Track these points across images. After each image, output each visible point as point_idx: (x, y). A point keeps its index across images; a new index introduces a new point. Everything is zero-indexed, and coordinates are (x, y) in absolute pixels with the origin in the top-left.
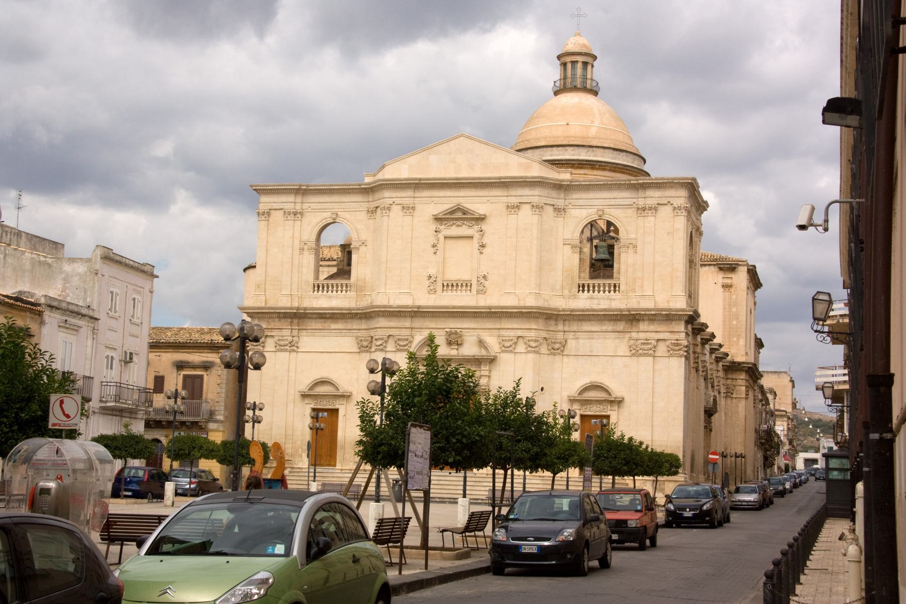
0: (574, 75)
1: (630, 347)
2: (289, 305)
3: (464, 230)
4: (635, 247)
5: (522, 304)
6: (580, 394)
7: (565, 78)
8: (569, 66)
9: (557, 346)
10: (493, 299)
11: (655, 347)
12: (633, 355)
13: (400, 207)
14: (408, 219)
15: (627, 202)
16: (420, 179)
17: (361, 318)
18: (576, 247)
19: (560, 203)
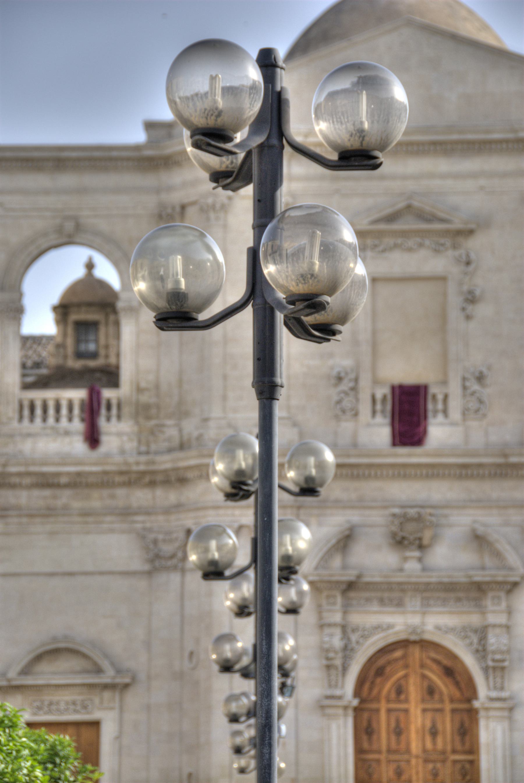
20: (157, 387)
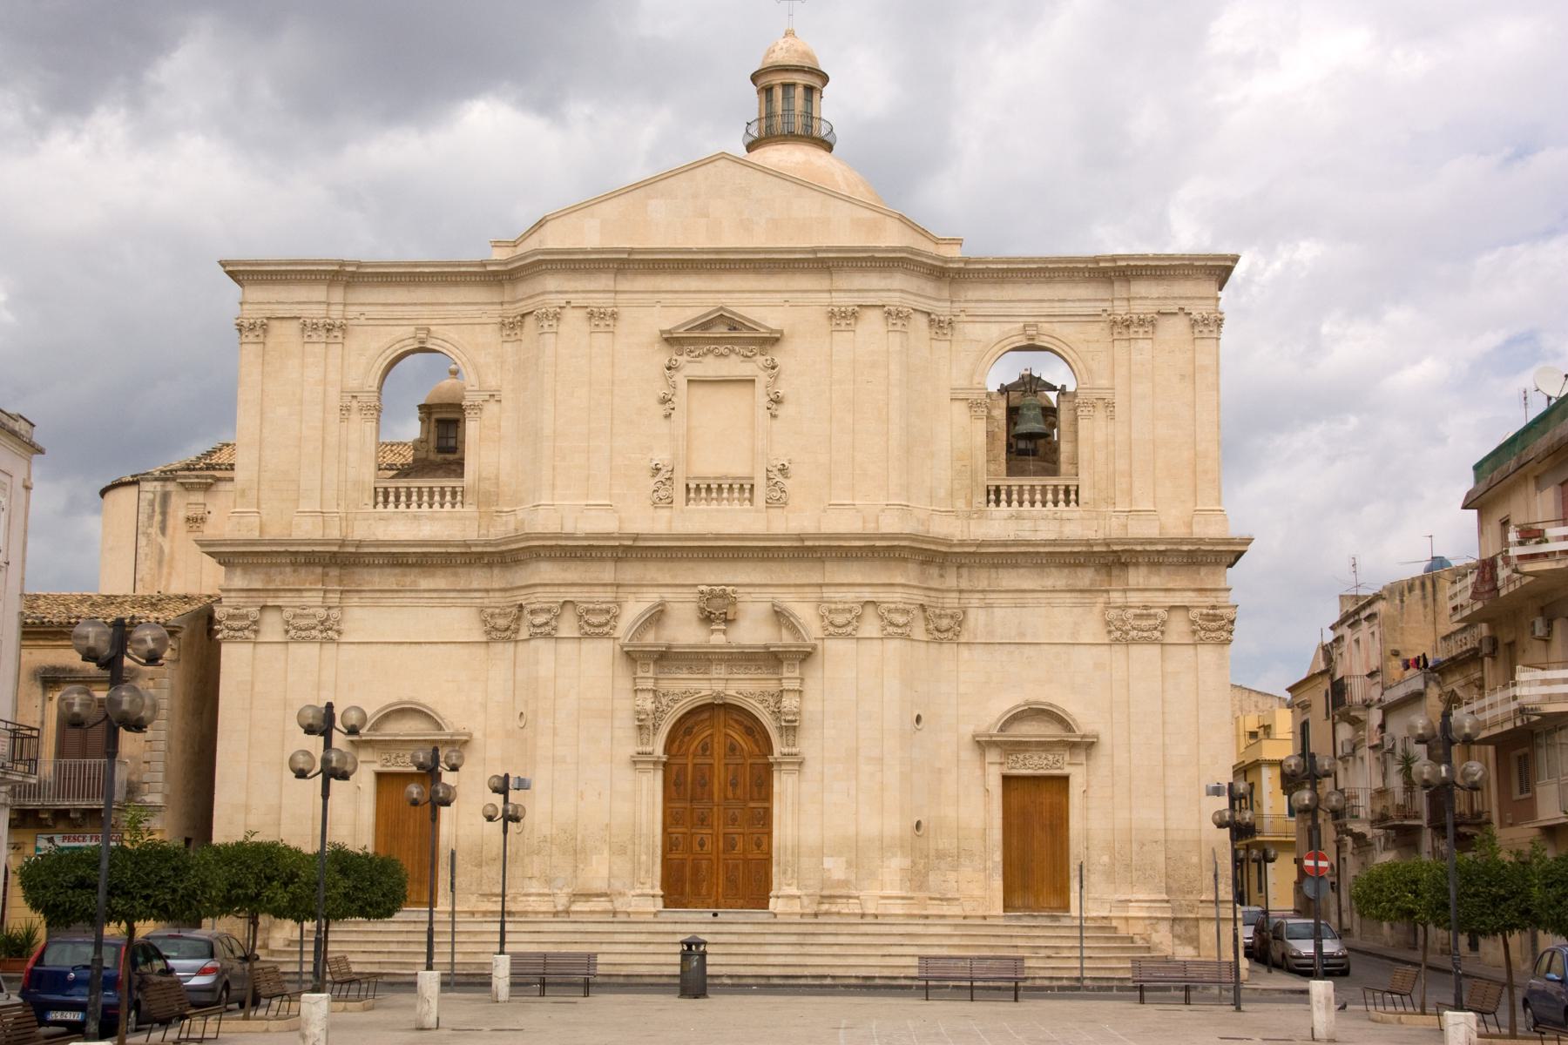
0: (788, 110)
1: (1108, 623)
2: (318, 535)
3: (734, 366)
4: (1109, 405)
5: (870, 528)
6: (1001, 730)
7: (770, 115)
8: (778, 93)
9: (945, 623)
10: (802, 518)
11: (1164, 623)
12: (1116, 641)
13: (582, 313)
14: (602, 340)
15: (1089, 308)
16: (631, 251)
17: (490, 565)
18: (979, 405)
19: (942, 309)
20: (497, 478)
